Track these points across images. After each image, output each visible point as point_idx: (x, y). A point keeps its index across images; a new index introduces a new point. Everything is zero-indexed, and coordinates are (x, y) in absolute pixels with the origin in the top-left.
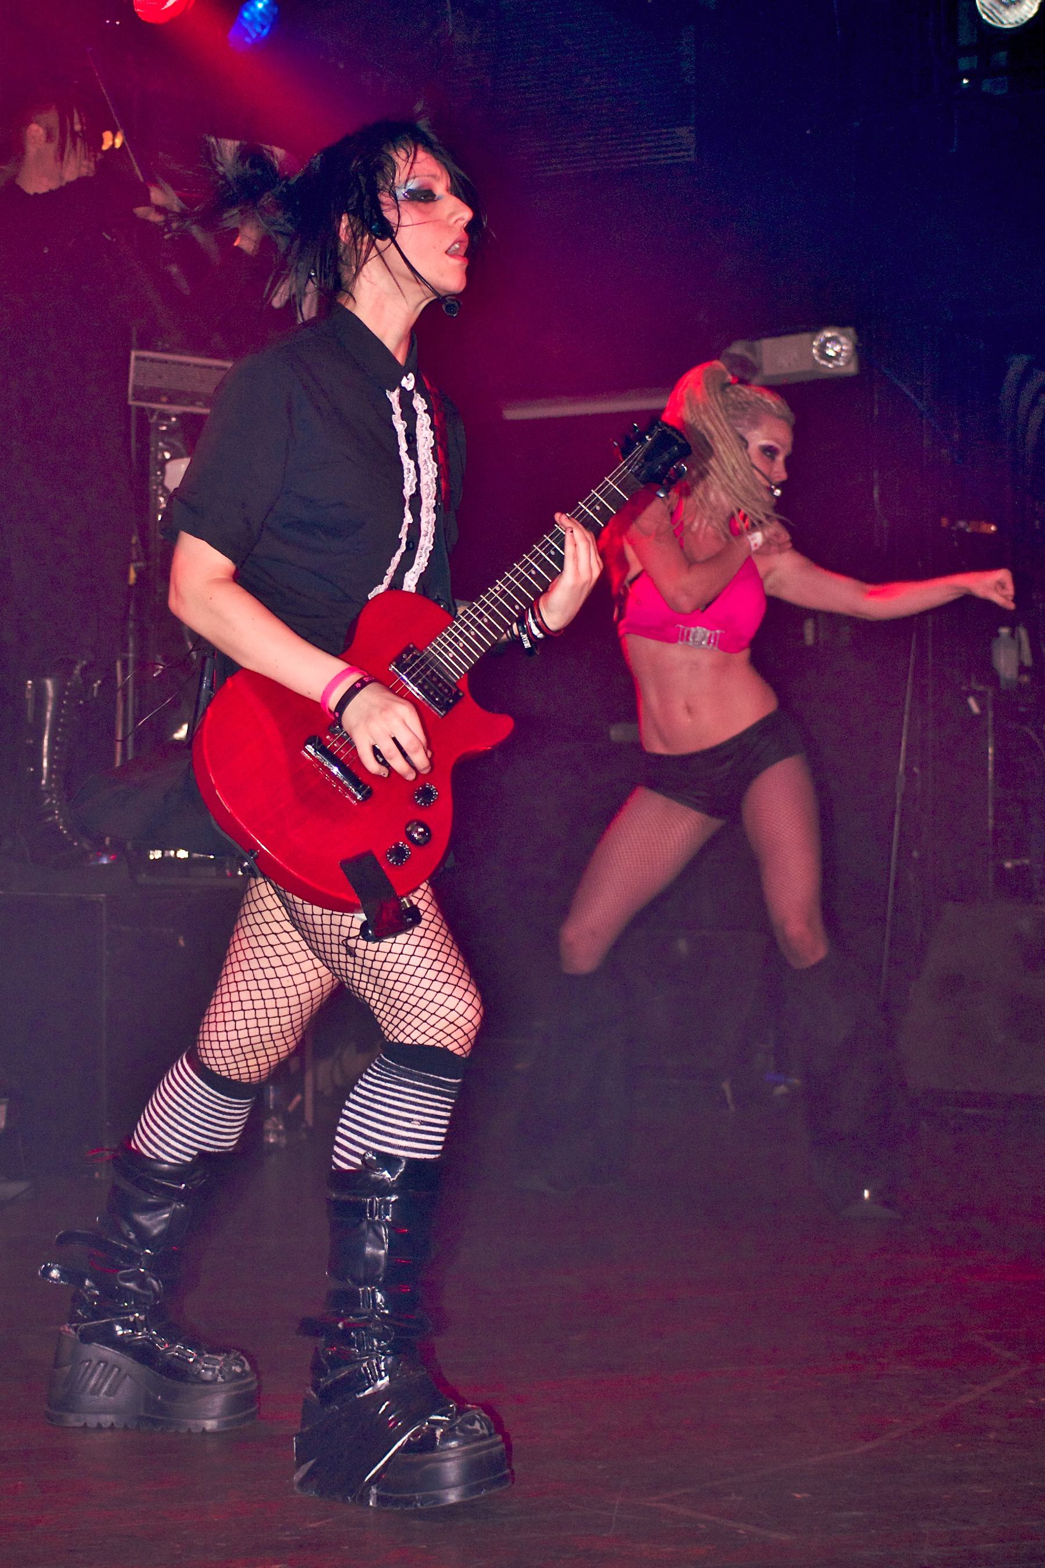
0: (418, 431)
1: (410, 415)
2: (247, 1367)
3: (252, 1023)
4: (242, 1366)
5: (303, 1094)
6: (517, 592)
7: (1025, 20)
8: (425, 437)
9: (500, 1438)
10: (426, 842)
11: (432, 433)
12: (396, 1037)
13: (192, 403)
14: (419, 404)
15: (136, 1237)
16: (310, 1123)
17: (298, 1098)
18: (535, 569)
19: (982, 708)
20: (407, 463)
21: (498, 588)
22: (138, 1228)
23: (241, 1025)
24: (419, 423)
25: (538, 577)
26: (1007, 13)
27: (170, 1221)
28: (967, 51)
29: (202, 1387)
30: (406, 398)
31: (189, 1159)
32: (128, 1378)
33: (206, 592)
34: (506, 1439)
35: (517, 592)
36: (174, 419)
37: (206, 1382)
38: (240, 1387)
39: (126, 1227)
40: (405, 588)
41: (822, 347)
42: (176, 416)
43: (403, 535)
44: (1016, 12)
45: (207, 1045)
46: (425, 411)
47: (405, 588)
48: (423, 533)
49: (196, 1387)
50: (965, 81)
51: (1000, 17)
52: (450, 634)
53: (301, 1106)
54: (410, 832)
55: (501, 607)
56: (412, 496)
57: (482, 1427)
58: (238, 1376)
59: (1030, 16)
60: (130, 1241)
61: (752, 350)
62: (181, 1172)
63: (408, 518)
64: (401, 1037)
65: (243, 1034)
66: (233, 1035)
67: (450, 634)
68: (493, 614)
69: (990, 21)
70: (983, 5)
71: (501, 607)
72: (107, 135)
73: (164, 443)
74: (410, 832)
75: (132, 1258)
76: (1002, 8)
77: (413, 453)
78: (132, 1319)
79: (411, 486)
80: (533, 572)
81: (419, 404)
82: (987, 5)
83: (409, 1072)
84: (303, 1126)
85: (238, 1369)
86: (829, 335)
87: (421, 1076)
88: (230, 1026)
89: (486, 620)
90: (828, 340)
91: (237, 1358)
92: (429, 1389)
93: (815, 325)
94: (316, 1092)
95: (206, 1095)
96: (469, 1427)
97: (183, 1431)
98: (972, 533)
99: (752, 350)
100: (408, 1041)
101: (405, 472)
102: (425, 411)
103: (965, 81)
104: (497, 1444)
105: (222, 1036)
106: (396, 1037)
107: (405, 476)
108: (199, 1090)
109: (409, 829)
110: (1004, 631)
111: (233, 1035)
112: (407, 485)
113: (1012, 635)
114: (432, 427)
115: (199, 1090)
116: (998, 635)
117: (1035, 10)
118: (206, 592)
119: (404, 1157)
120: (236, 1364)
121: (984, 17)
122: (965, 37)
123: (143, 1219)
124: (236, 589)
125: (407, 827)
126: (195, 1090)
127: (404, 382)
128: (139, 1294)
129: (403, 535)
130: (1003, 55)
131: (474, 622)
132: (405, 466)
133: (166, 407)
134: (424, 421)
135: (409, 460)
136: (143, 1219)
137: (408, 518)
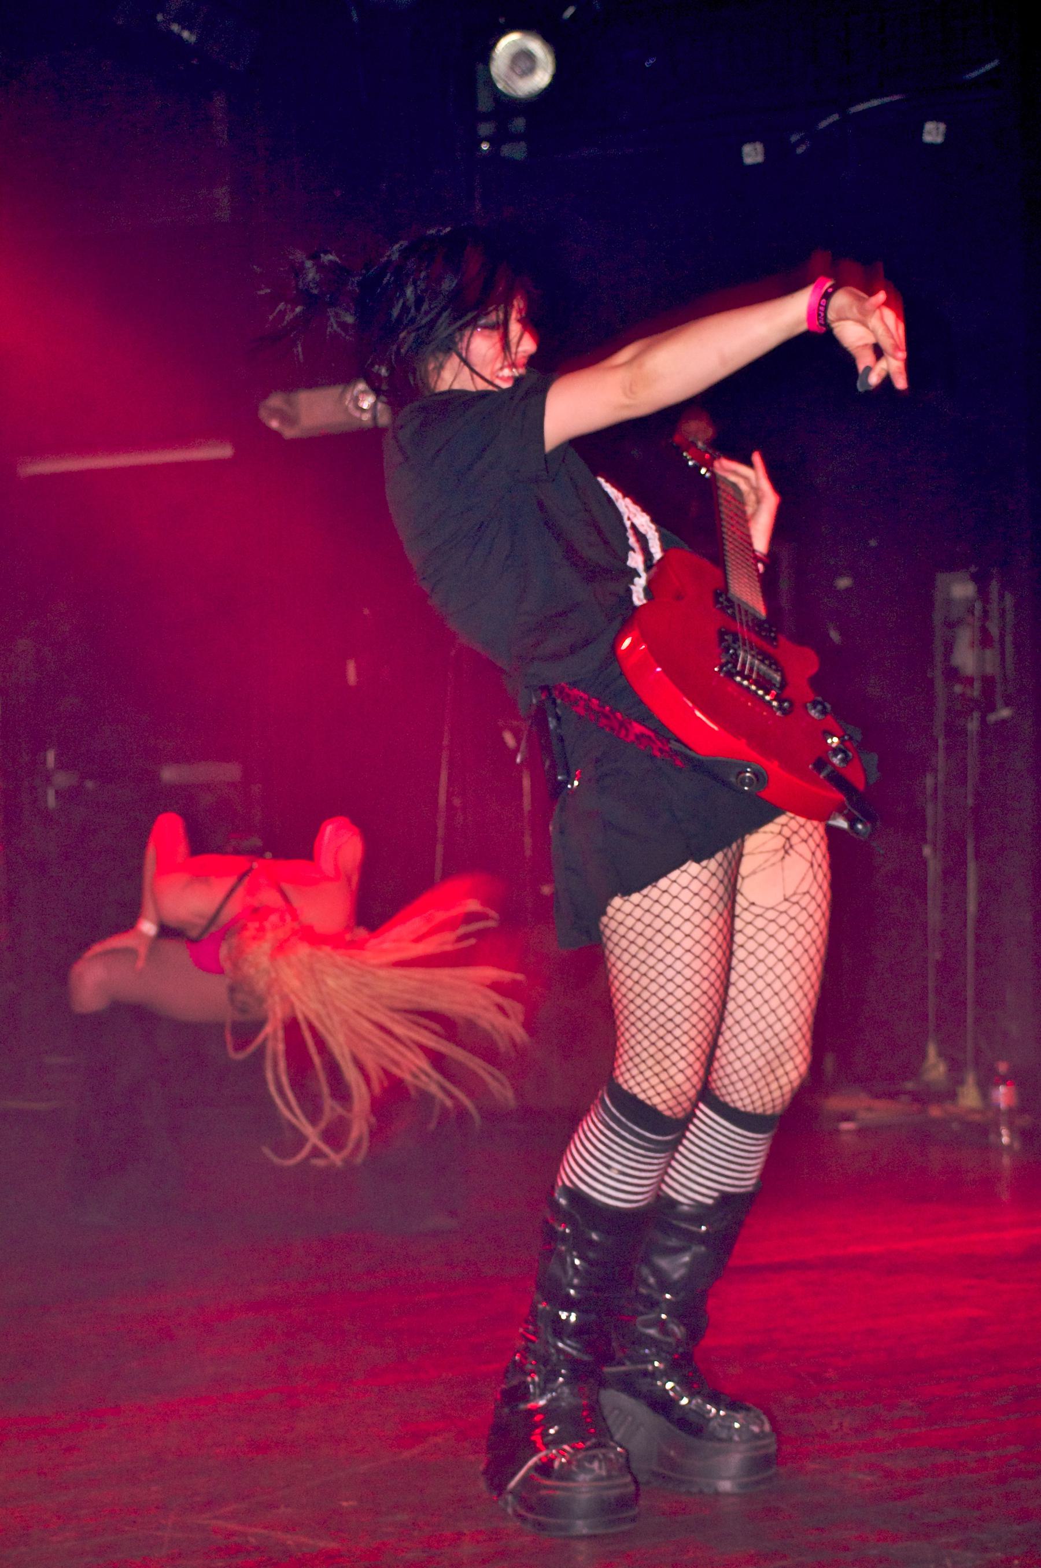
2: (767, 1427)
3: (759, 1040)
4: (761, 1426)
15: (657, 1282)
19: (518, 741)
22: (657, 1272)
23: (749, 1046)
27: (690, 1265)
28: (486, 117)
29: (717, 1445)
31: (710, 1201)
32: (642, 1429)
37: (720, 1440)
38: (756, 1449)
39: (645, 1271)
41: (356, 400)
45: (719, 1084)
49: (710, 1444)
57: (600, 1468)
58: (756, 1437)
60: (649, 1286)
61: (289, 403)
62: (701, 1214)
65: (756, 1054)
66: (747, 1060)
72: (930, 126)
75: (653, 1304)
78: (650, 1368)
85: (756, 1429)
88: (740, 1052)
91: (758, 1417)
93: (347, 379)
97: (695, 1490)
99: (289, 403)
104: (626, 1485)
105: (737, 1065)
111: (747, 1060)
122: (485, 104)
123: (663, 1263)
128: (661, 1342)
136: (663, 1263)
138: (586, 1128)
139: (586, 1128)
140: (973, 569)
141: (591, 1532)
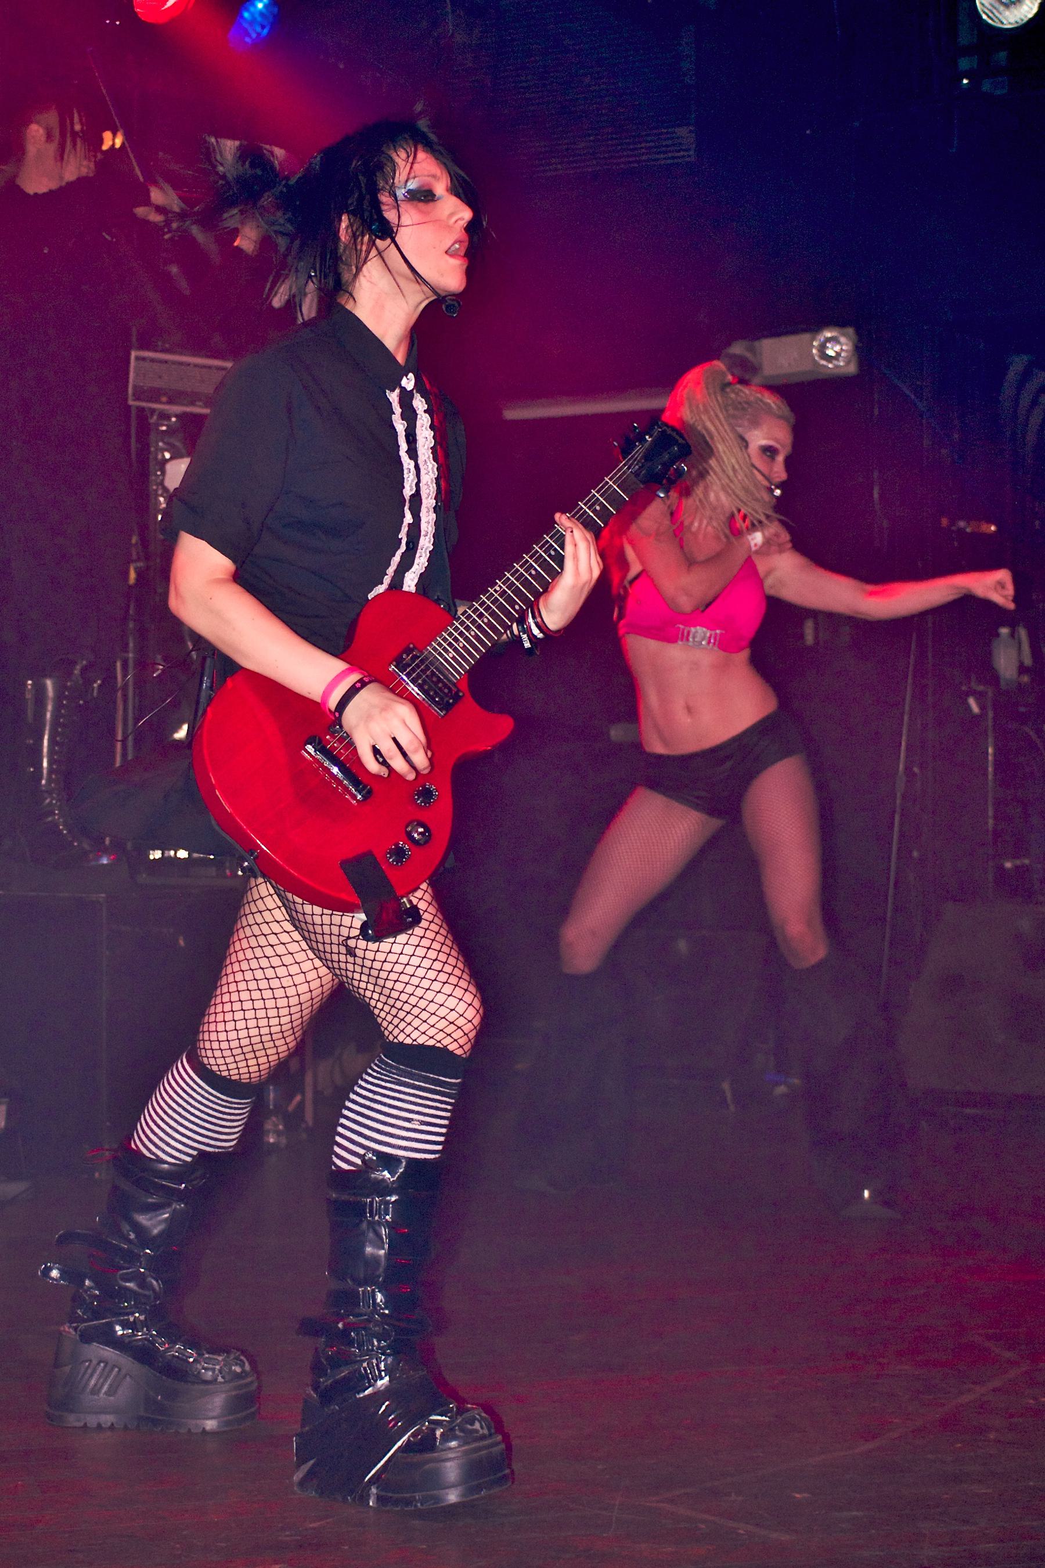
0: (418, 431)
1: (410, 415)
2: (247, 1367)
3: (252, 1023)
4: (242, 1366)
5: (303, 1094)
6: (517, 592)
7: (1025, 20)
8: (425, 437)
9: (500, 1438)
10: (426, 842)
11: (432, 433)
12: (396, 1037)
13: (192, 403)
14: (419, 404)
15: (136, 1237)
16: (310, 1123)
17: (298, 1098)
18: (535, 569)
20: (407, 463)
21: (498, 588)
22: (138, 1228)
23: (241, 1025)
24: (419, 423)
25: (538, 577)
26: (1007, 13)
27: (170, 1221)
28: (967, 51)
29: (202, 1387)
30: (406, 398)
31: (189, 1159)
32: (128, 1378)
33: (206, 592)
34: (506, 1439)
35: (517, 592)
36: (174, 419)
37: (206, 1382)
38: (240, 1387)
39: (126, 1227)
40: (405, 588)
42: (176, 416)
43: (403, 535)
44: (1016, 12)
46: (425, 411)
47: (405, 588)
48: (423, 533)
49: (196, 1387)
50: (965, 81)
51: (1000, 17)
52: (450, 634)
53: (301, 1106)
54: (410, 832)
55: (501, 607)
56: (412, 496)
57: (482, 1427)
58: (238, 1376)
59: (1030, 16)
60: (130, 1241)
61: (752, 350)
62: (181, 1172)
63: (408, 518)
64: (401, 1037)
65: (243, 1034)
66: (233, 1035)
67: (450, 634)
68: (493, 614)
69: (990, 21)
70: (983, 5)
71: (501, 607)
72: (107, 135)
73: (164, 443)
74: (410, 832)
75: (132, 1258)
76: (1002, 8)
77: (413, 453)
78: (132, 1319)
79: (411, 486)
80: (533, 572)
81: (419, 404)
82: (987, 5)
83: (409, 1072)
84: (303, 1126)
85: (238, 1369)
86: (829, 335)
87: (421, 1076)
88: (230, 1026)
89: (486, 620)
90: (828, 340)
91: (237, 1358)
92: (429, 1389)
94: (316, 1092)
95: (206, 1095)
96: (469, 1427)
97: (183, 1431)
98: (972, 533)
99: (752, 350)
100: (408, 1041)
101: (405, 472)
102: (425, 411)
103: (965, 81)
105: (222, 1036)
106: (396, 1037)
107: (405, 476)
108: (199, 1090)
109: (409, 829)
110: (1004, 631)
111: (233, 1035)
112: (407, 485)
113: (1012, 635)
114: (432, 427)
115: (199, 1090)
116: (998, 635)
117: (1035, 10)
118: (206, 592)
119: (404, 1157)
120: (236, 1364)
121: (984, 17)
122: (965, 37)
123: (143, 1219)
124: (236, 589)
125: (407, 827)
126: (195, 1090)
127: (404, 382)
128: (139, 1294)
129: (403, 535)
130: (1003, 55)
131: (474, 622)
132: (405, 466)
133: (166, 407)
134: (424, 421)
135: (409, 460)
136: (143, 1219)
137: (408, 518)
138: (175, 1072)
139: (175, 1072)
140: (617, 733)
141: (443, 1464)
